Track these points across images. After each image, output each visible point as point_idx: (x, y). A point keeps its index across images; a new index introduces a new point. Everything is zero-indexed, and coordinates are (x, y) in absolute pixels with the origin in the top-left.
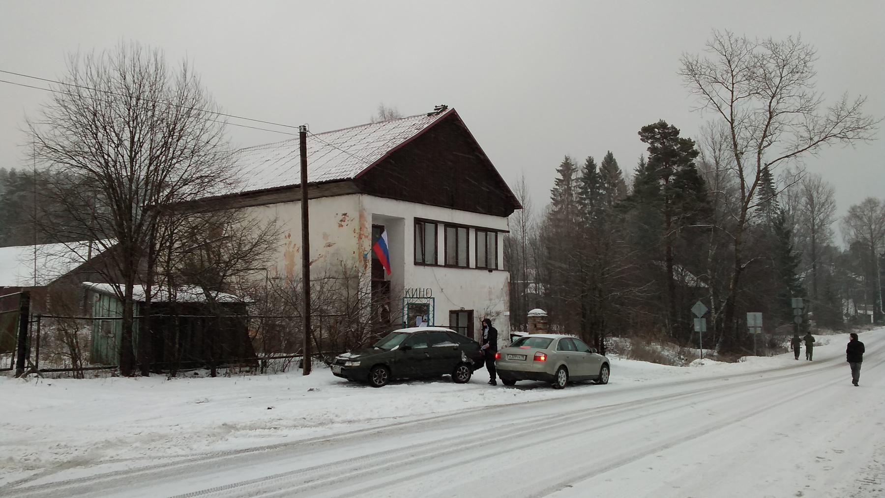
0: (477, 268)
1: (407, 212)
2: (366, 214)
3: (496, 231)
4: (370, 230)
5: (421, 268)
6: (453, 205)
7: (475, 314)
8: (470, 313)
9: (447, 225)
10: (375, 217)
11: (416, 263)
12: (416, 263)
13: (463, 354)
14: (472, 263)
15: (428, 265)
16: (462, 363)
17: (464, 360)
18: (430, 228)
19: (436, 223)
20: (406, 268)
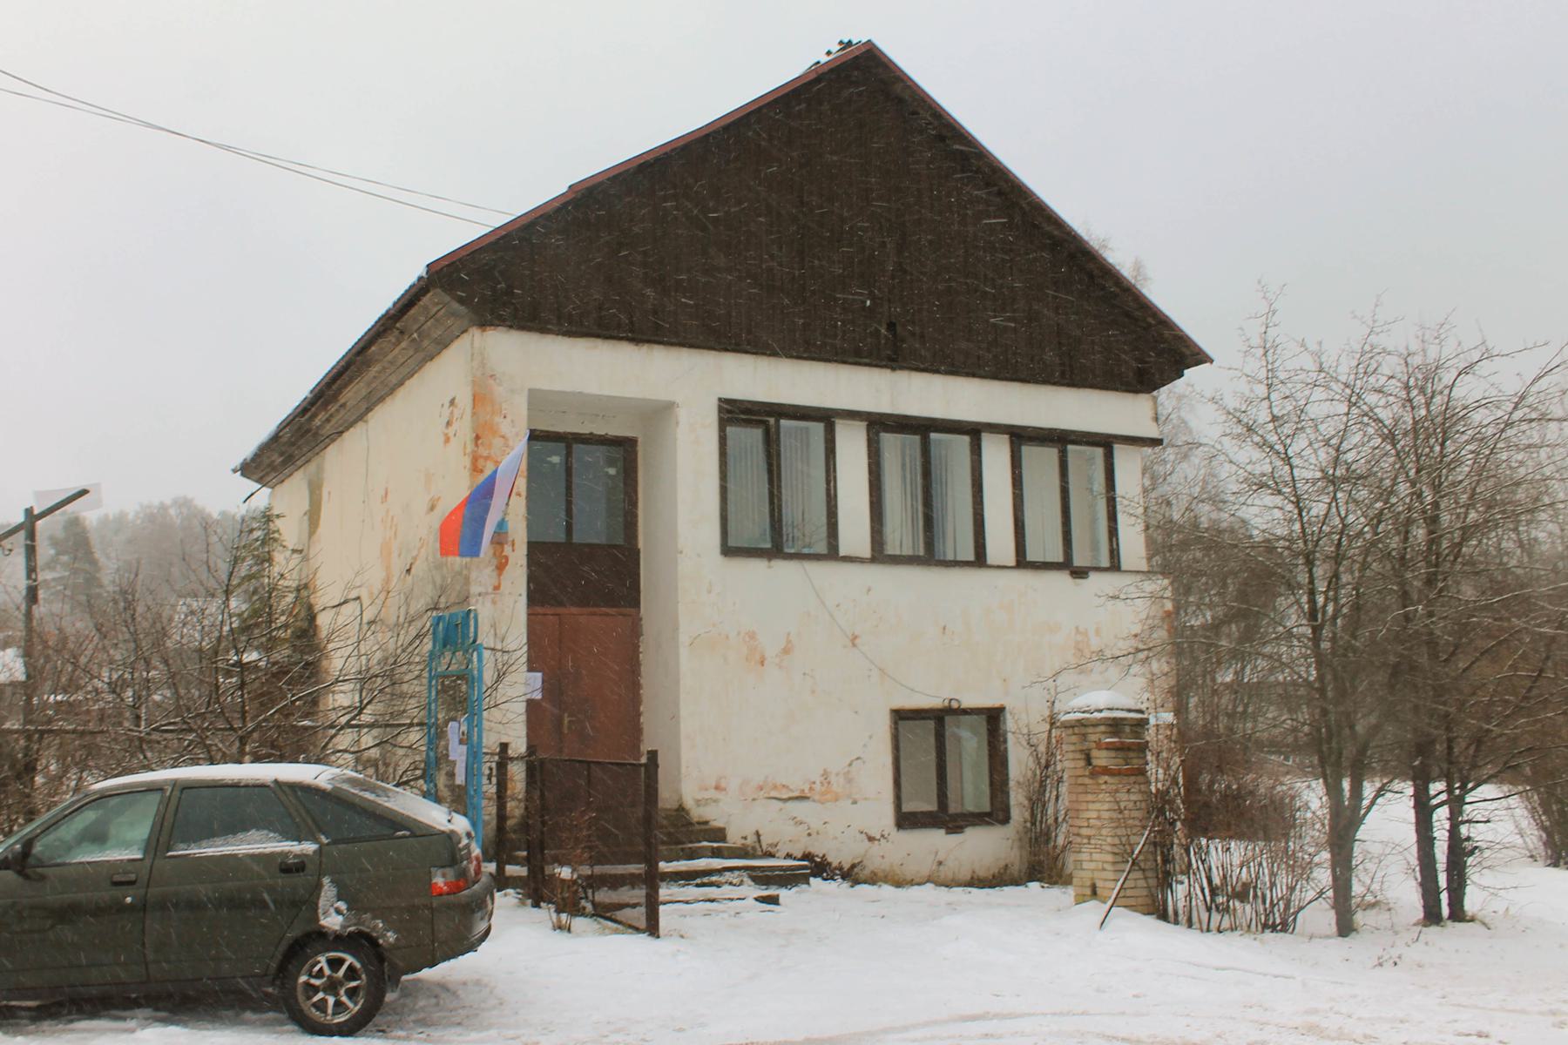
0: (879, 555)
1: (680, 391)
2: (499, 391)
3: (1106, 443)
4: (520, 446)
5: (756, 568)
6: (892, 354)
7: (1010, 724)
8: (993, 717)
9: (878, 424)
10: (537, 399)
11: (728, 551)
12: (728, 551)
13: (328, 891)
14: (1000, 543)
15: (956, 564)
16: (321, 938)
17: (332, 921)
18: (800, 441)
19: (974, 432)
20: (685, 566)
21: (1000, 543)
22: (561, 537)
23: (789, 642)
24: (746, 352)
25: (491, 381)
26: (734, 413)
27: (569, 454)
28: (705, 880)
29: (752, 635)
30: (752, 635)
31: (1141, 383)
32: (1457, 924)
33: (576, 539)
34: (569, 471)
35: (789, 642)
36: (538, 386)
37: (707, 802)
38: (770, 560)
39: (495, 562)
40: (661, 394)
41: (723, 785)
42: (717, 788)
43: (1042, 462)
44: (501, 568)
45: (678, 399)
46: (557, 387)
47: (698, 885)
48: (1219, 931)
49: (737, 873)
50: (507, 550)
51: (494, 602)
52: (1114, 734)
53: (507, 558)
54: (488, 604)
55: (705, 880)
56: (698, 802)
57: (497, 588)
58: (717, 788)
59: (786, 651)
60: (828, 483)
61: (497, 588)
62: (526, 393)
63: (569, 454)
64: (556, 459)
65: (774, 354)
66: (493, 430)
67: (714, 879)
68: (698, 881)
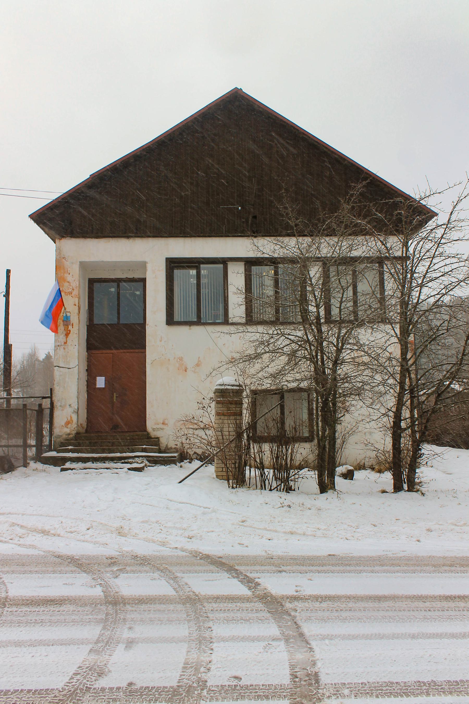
2: (67, 264)
10: (84, 266)
21: (237, 310)
22: (115, 321)
23: (199, 361)
24: (149, 237)
25: (64, 260)
26: (173, 264)
27: (118, 286)
28: (126, 461)
29: (181, 359)
30: (181, 359)
31: (397, 231)
32: (410, 493)
33: (121, 322)
34: (118, 294)
35: (199, 361)
36: (83, 260)
37: (158, 429)
38: (190, 326)
39: (65, 332)
40: (139, 259)
41: (166, 422)
42: (163, 424)
43: (268, 271)
44: (67, 335)
45: (147, 260)
46: (92, 259)
47: (122, 463)
48: (271, 490)
49: (141, 458)
50: (70, 327)
51: (64, 349)
52: (223, 397)
53: (70, 331)
54: (62, 350)
55: (126, 461)
56: (154, 429)
57: (65, 343)
58: (163, 424)
59: (198, 365)
60: (224, 290)
61: (65, 343)
62: (79, 263)
63: (118, 286)
64: (113, 290)
65: (191, 236)
66: (64, 280)
67: (130, 460)
68: (123, 461)
